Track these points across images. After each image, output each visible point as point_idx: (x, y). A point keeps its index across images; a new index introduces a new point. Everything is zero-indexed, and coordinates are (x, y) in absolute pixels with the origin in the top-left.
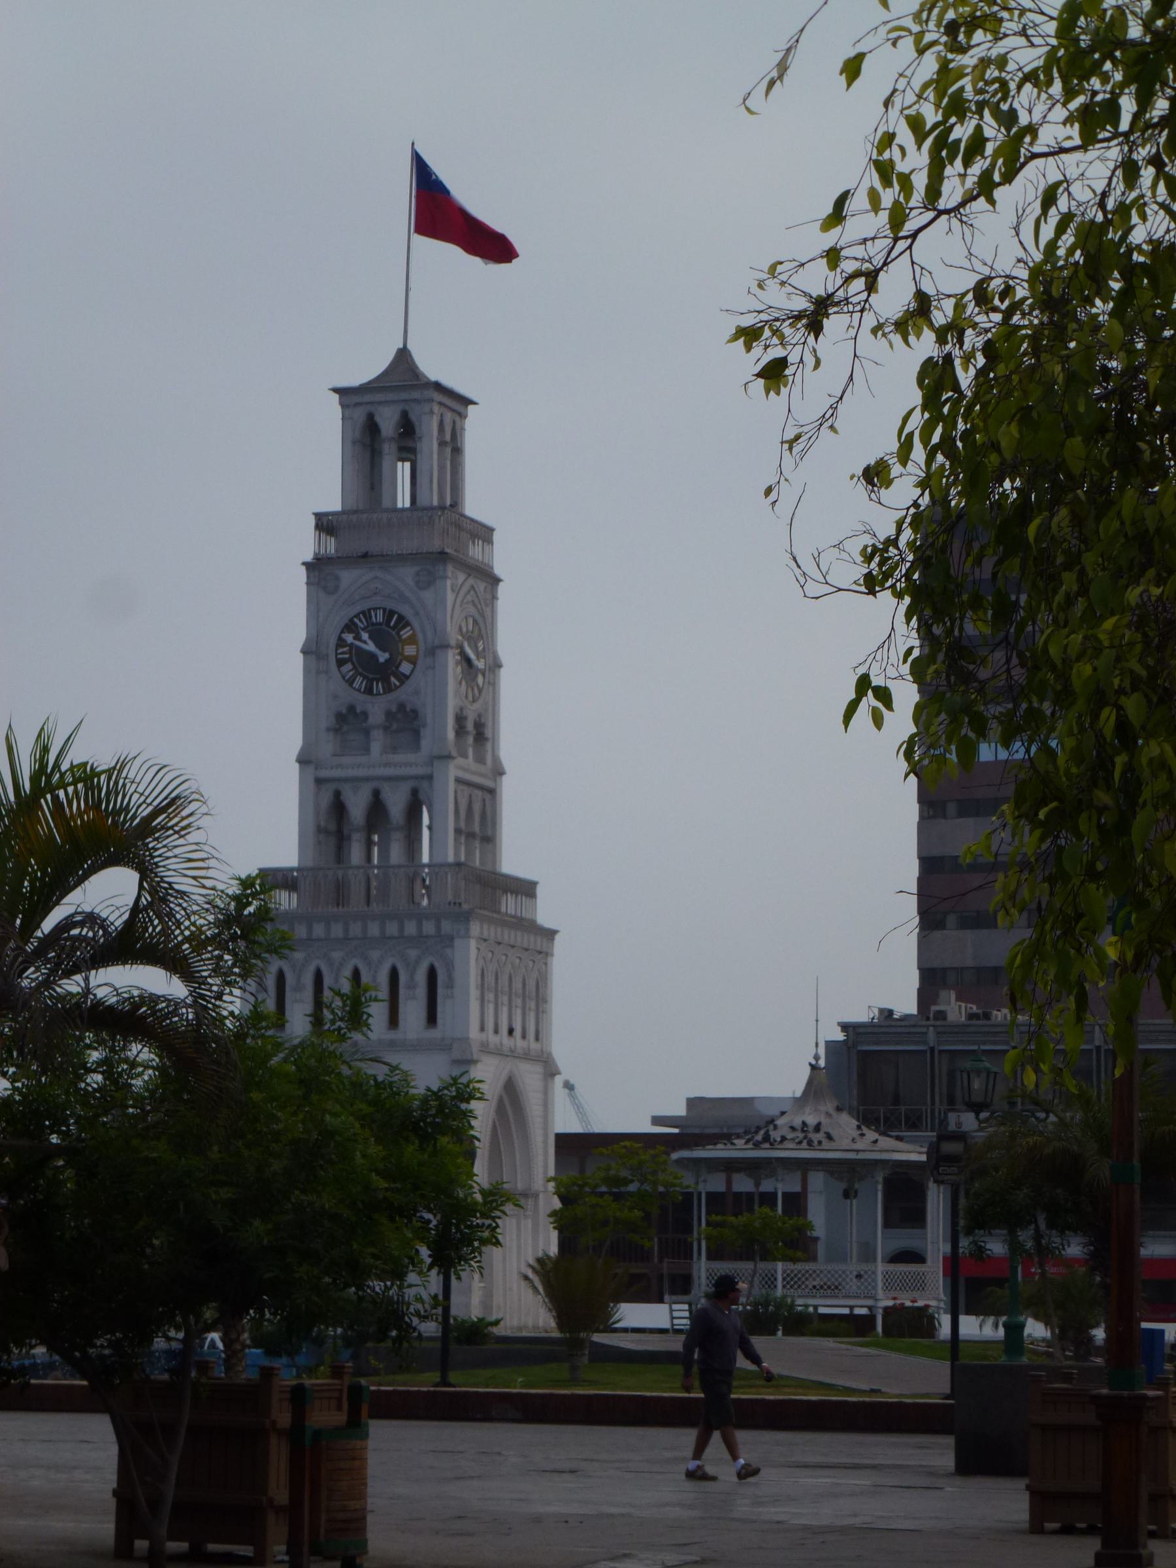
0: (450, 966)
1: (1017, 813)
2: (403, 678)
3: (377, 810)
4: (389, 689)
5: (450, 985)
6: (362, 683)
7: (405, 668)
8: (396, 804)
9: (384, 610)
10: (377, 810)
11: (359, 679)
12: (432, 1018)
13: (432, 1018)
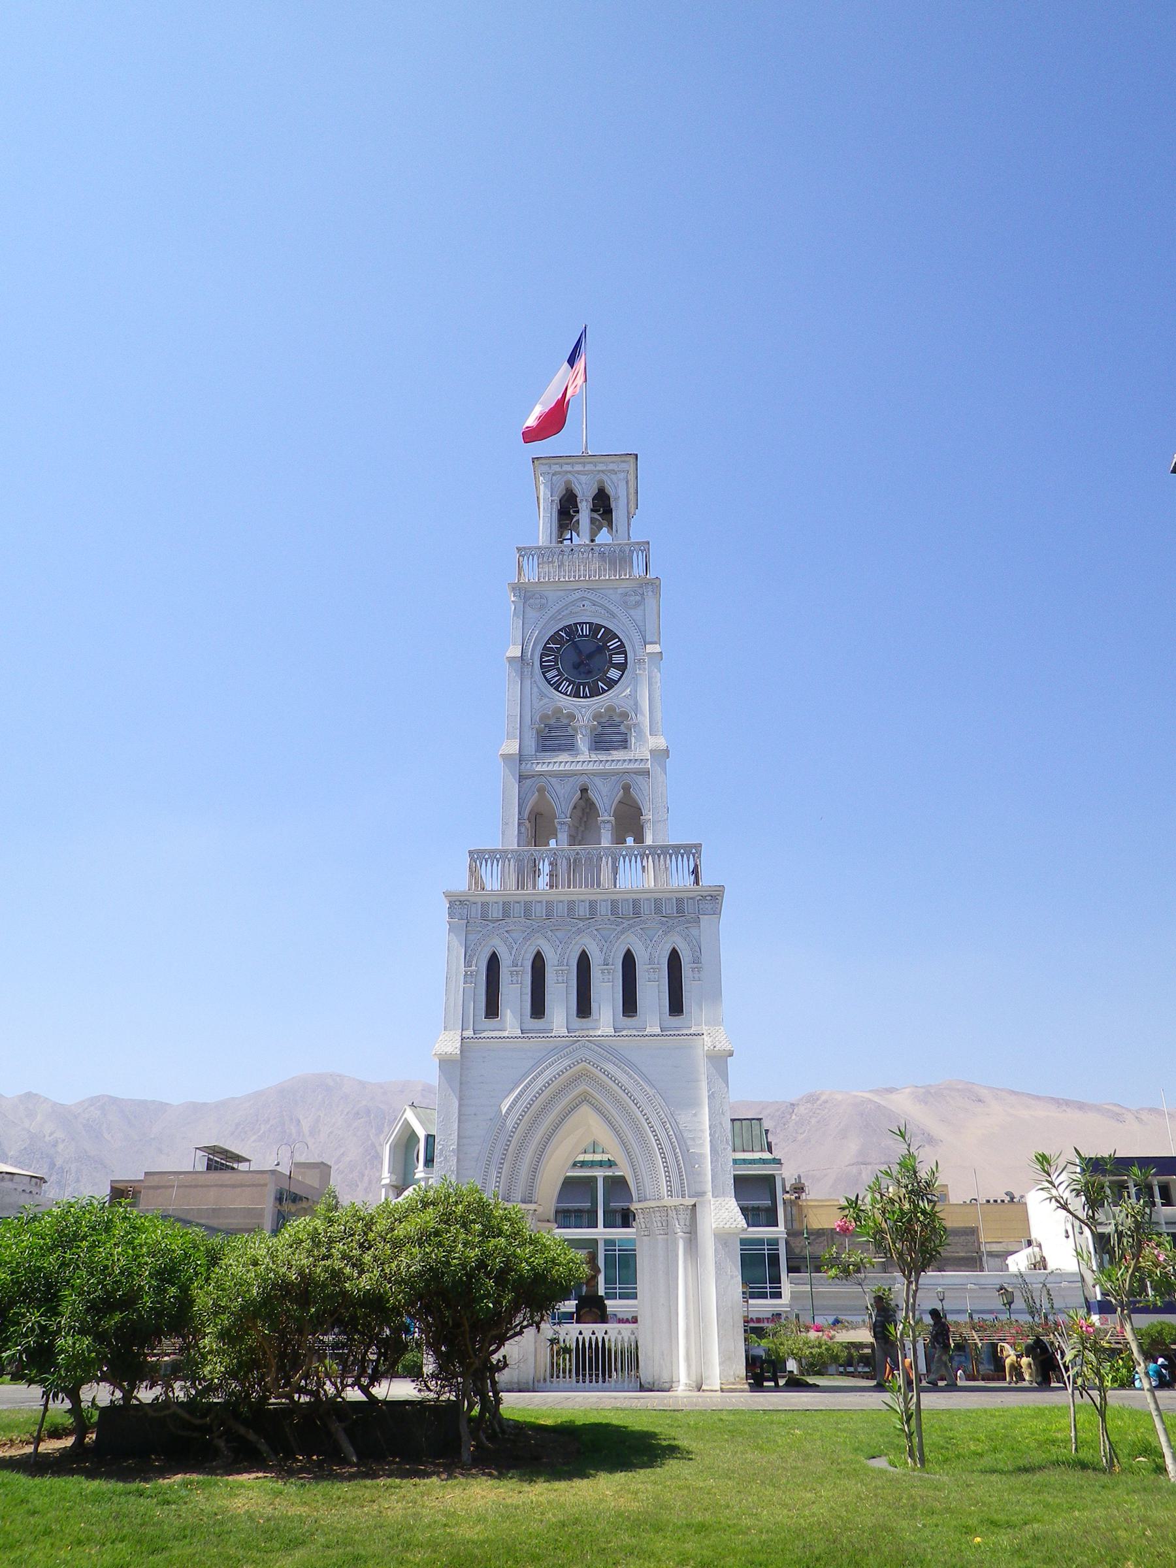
0: (697, 949)
1: (493, 880)
3: (586, 809)
4: (596, 692)
5: (697, 960)
6: (568, 686)
8: (605, 799)
10: (586, 809)
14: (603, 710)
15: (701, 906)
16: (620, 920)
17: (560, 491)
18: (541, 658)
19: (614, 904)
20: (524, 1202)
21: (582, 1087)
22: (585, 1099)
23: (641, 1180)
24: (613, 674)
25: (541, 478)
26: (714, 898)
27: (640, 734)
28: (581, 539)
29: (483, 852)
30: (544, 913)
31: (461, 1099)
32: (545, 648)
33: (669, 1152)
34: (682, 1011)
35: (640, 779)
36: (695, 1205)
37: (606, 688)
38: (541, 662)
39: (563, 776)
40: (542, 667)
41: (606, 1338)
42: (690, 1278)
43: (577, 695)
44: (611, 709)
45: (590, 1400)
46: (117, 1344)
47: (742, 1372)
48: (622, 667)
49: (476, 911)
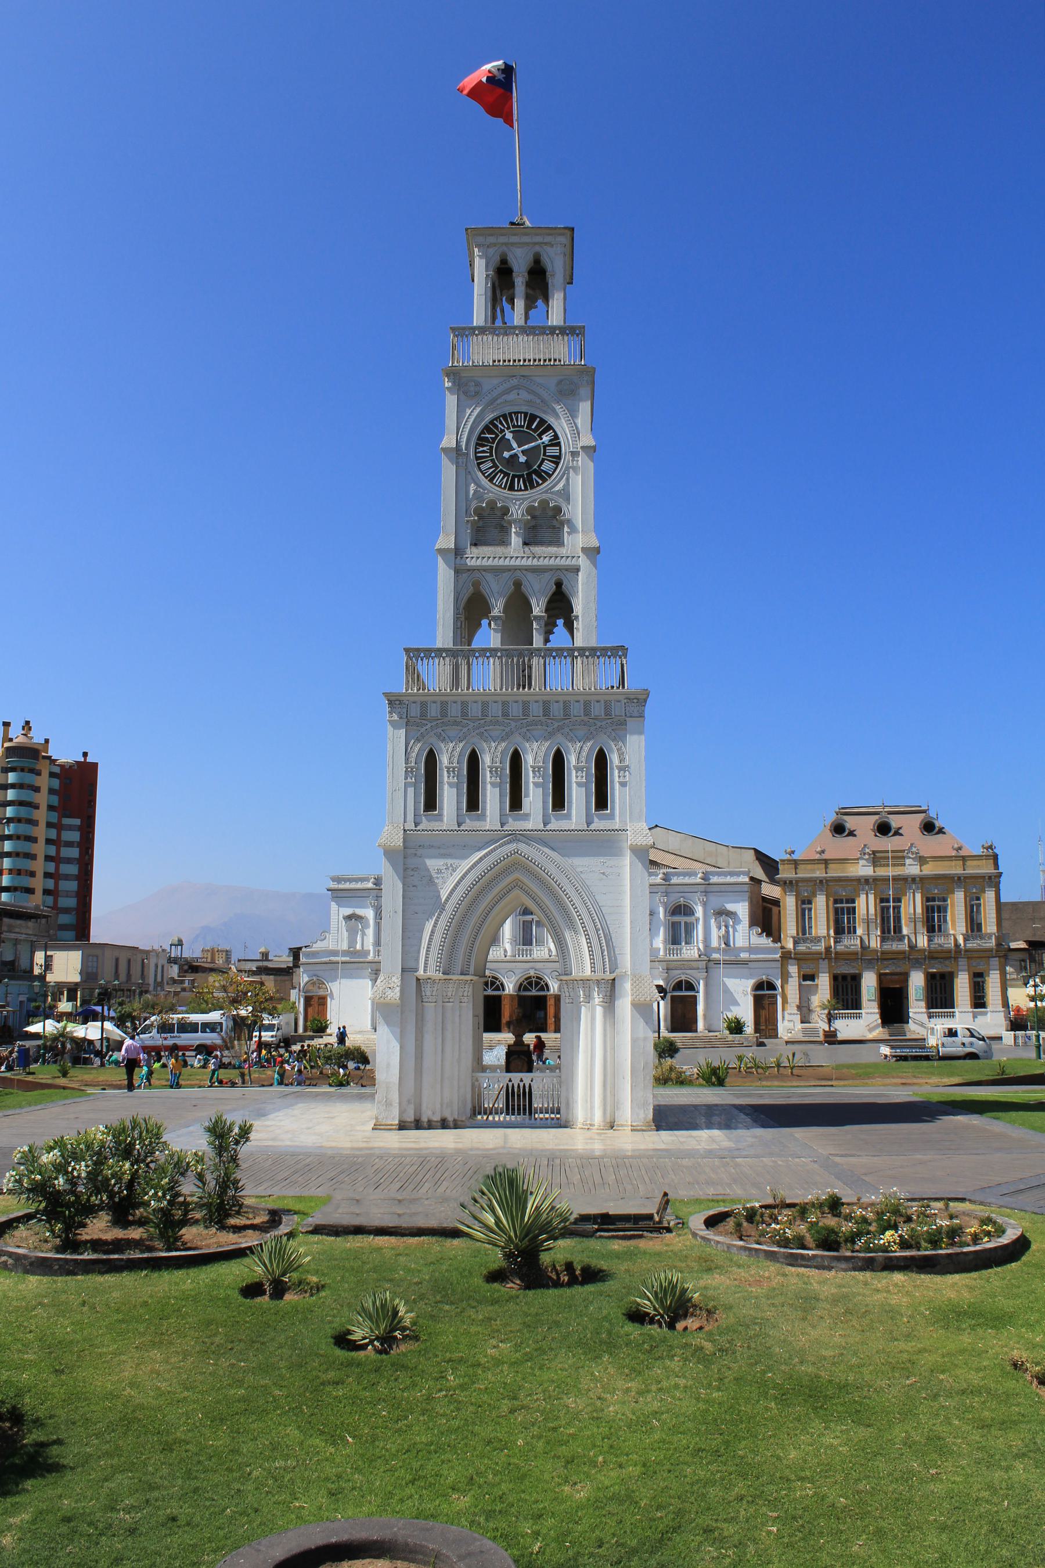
2: (544, 476)
4: (530, 484)
7: (547, 466)
9: (479, 464)
11: (500, 476)
12: (117, 960)
13: (117, 960)
14: (536, 505)
15: (627, 708)
16: (550, 721)
17: (497, 259)
18: (476, 448)
19: (546, 706)
20: (462, 974)
21: (516, 875)
22: (517, 885)
23: (544, 906)
24: (547, 466)
25: (476, 250)
26: (640, 700)
27: (573, 530)
28: (517, 315)
29: (418, 650)
30: (480, 714)
31: (404, 885)
32: (480, 438)
33: (593, 934)
34: (654, 1110)
35: (570, 575)
36: (614, 979)
37: (541, 482)
38: (476, 453)
39: (497, 571)
40: (477, 458)
41: (521, 1085)
42: (608, 1036)
43: (511, 488)
44: (544, 503)
45: (184, 1009)
46: (874, 1243)
47: (651, 1116)
48: (556, 460)
49: (415, 711)
